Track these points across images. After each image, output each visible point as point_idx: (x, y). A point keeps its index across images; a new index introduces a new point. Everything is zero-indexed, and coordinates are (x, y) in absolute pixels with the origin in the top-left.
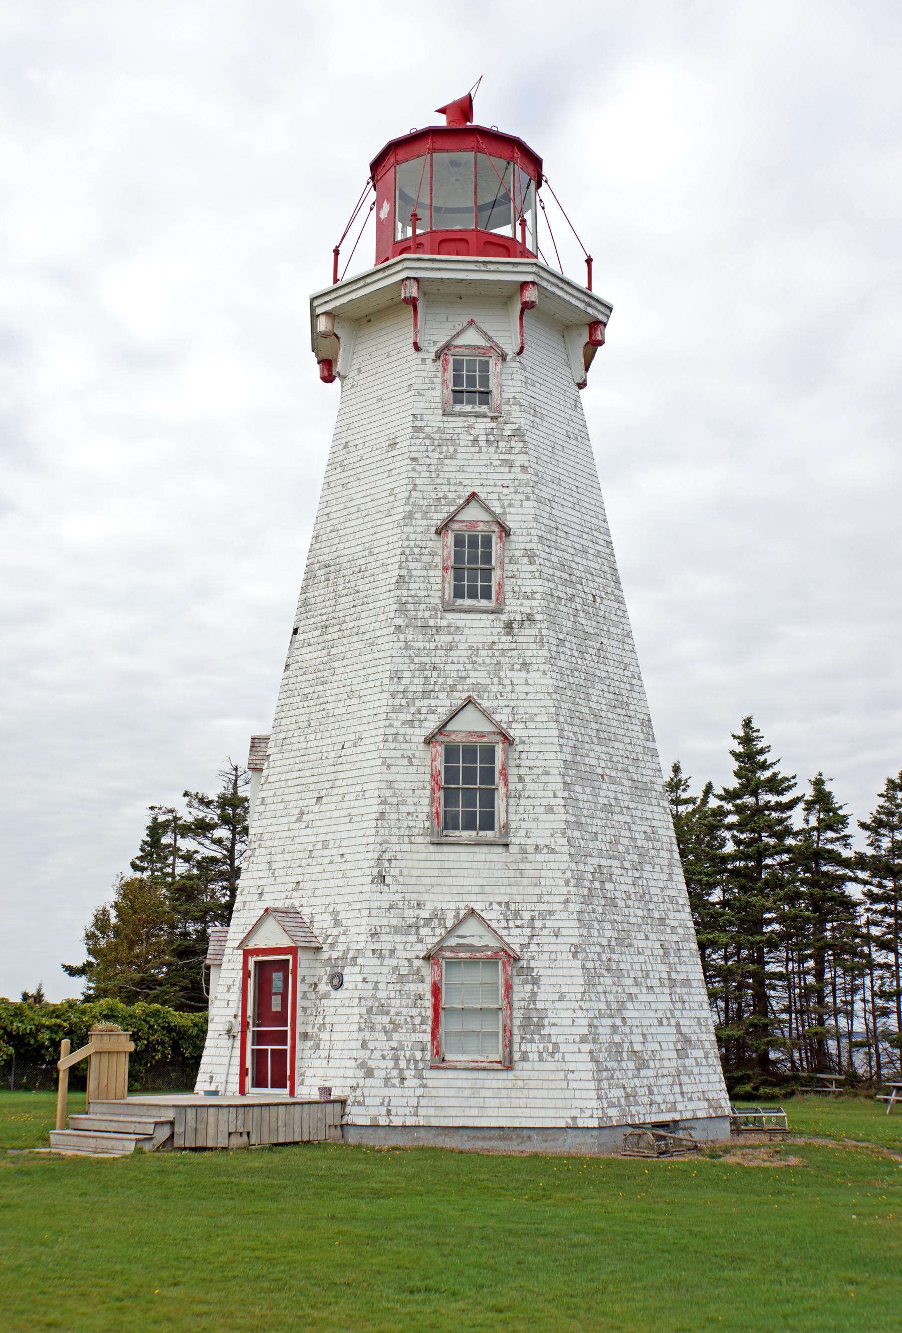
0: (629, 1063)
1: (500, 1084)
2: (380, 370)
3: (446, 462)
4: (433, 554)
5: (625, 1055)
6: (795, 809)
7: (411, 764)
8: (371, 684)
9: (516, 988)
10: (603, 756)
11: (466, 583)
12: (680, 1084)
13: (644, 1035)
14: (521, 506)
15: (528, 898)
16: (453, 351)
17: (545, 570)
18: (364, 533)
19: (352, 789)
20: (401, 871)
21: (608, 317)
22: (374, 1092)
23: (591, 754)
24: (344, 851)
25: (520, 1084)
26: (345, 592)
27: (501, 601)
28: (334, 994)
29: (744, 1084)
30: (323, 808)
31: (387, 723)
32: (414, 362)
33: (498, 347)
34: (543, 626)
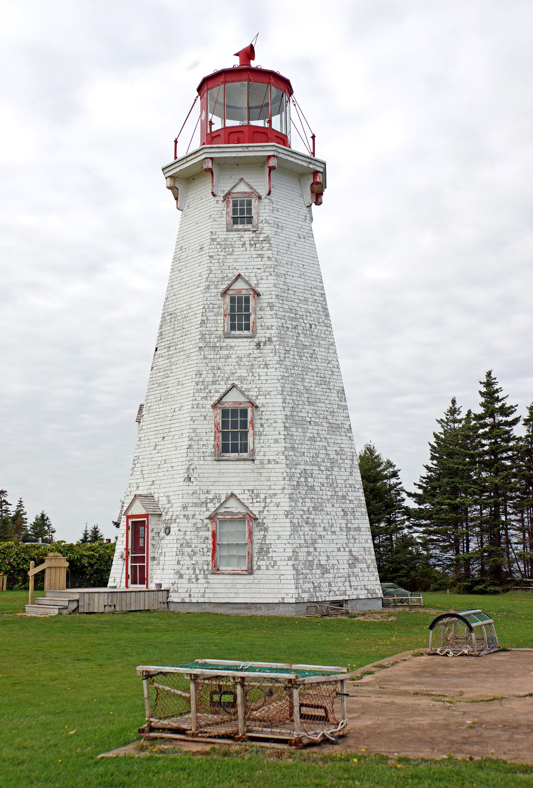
0: (317, 571)
1: (246, 582)
2: (198, 206)
3: (228, 257)
4: (219, 307)
5: (315, 567)
6: (517, 425)
7: (205, 419)
8: (187, 378)
9: (254, 534)
10: (311, 411)
11: (236, 322)
12: (350, 582)
13: (328, 556)
14: (267, 279)
15: (264, 487)
16: (232, 196)
17: (279, 313)
18: (187, 297)
19: (177, 433)
20: (199, 475)
21: (164, 174)
22: (183, 586)
23: (303, 411)
24: (173, 465)
25: (256, 581)
26: (178, 328)
27: (255, 333)
28: (167, 537)
29: (481, 585)
30: (165, 442)
31: (194, 398)
32: (212, 203)
33: (256, 192)
34: (276, 344)
